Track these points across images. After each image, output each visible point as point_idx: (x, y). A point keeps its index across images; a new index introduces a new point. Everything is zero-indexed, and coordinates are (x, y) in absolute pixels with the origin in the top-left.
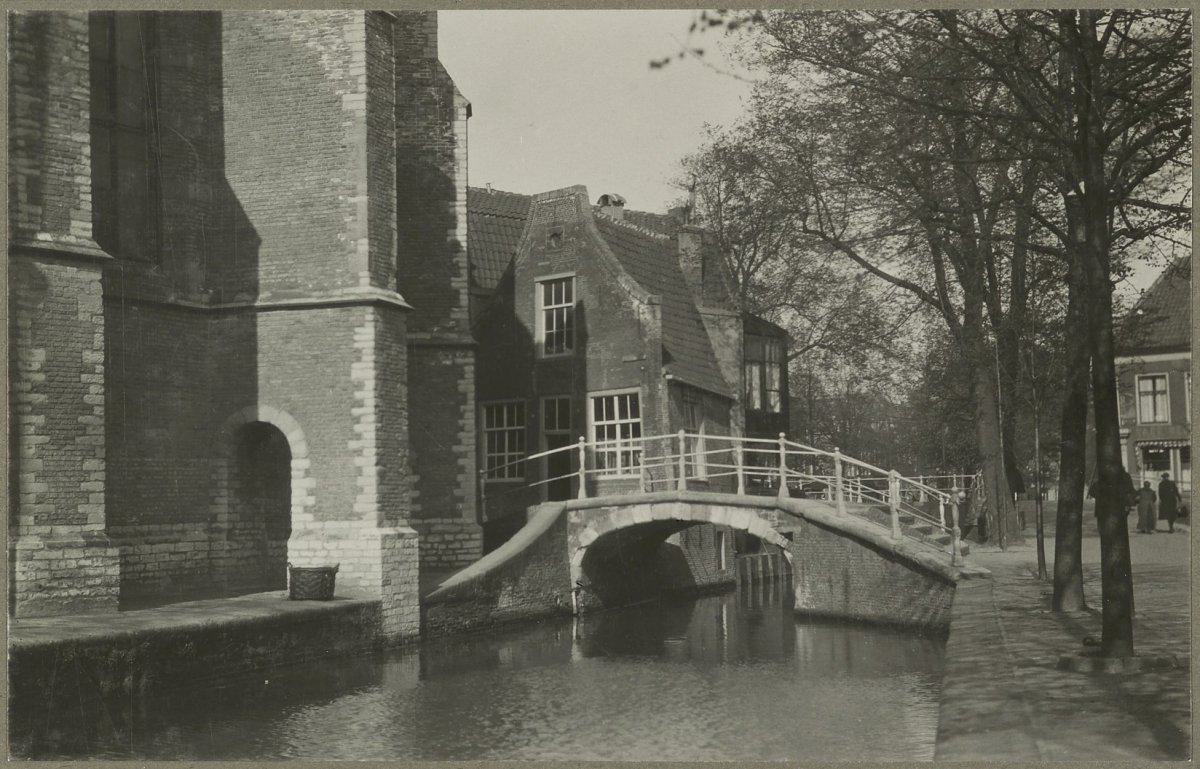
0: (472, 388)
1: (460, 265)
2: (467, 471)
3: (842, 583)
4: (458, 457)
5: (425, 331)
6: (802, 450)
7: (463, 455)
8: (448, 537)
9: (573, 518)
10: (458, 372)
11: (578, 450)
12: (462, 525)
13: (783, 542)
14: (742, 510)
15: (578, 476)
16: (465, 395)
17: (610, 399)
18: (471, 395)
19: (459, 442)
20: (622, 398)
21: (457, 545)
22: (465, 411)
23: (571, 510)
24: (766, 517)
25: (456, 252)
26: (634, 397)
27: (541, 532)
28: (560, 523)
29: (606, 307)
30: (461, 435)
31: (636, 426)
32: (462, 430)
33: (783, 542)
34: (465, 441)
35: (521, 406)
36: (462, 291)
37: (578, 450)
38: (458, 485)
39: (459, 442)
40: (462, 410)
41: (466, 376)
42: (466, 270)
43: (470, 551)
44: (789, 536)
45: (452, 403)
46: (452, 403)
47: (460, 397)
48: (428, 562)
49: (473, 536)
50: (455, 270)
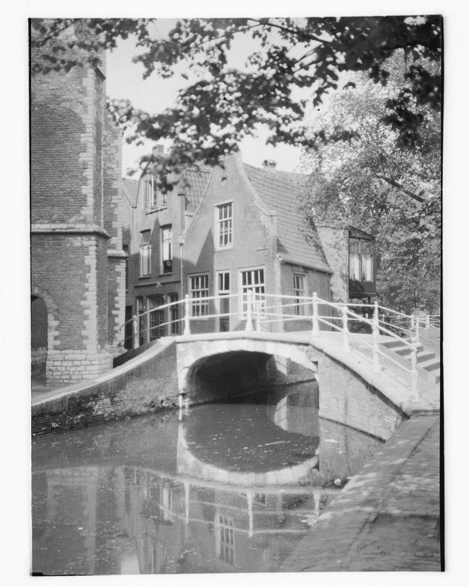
0: (95, 261)
1: (88, 177)
2: (90, 318)
3: (344, 402)
4: (85, 309)
5: (64, 222)
6: (290, 318)
7: (88, 308)
8: (76, 363)
9: (180, 348)
10: (84, 250)
11: (184, 304)
12: (87, 354)
13: (312, 367)
14: (287, 346)
15: (184, 321)
16: (89, 267)
17: (249, 273)
18: (93, 267)
19: (85, 299)
20: (256, 272)
21: (82, 368)
22: (89, 277)
23: (178, 343)
24: (302, 350)
25: (85, 168)
26: (262, 271)
27: (152, 358)
28: (171, 351)
29: (248, 219)
30: (86, 293)
31: (263, 288)
32: (87, 290)
33: (312, 367)
34: (88, 298)
35: (207, 277)
36: (89, 195)
37: (184, 304)
38: (84, 328)
39: (85, 299)
40: (87, 277)
41: (90, 253)
42: (92, 181)
43: (91, 372)
44: (316, 363)
45: (81, 272)
46: (81, 272)
47: (87, 268)
48: (63, 380)
49: (93, 363)
50: (84, 181)
